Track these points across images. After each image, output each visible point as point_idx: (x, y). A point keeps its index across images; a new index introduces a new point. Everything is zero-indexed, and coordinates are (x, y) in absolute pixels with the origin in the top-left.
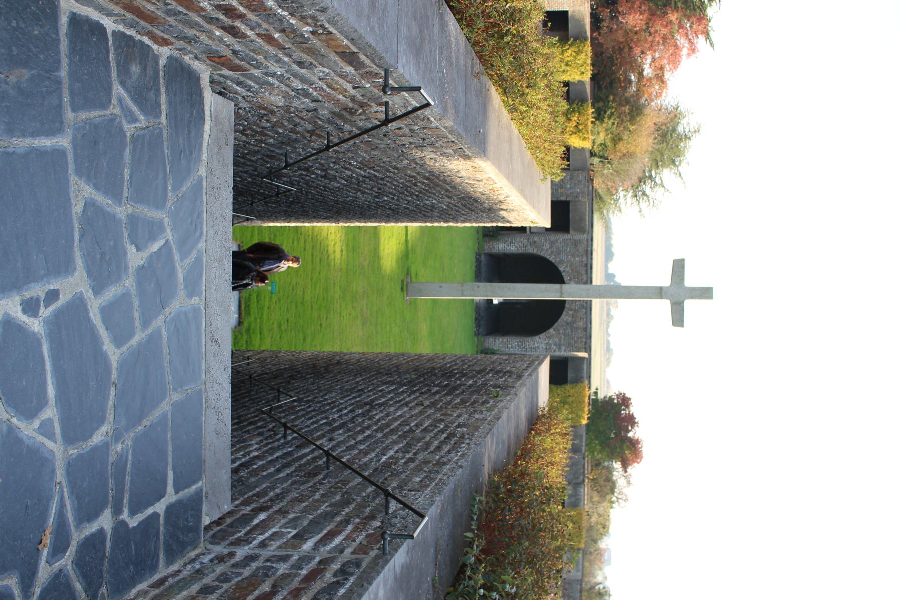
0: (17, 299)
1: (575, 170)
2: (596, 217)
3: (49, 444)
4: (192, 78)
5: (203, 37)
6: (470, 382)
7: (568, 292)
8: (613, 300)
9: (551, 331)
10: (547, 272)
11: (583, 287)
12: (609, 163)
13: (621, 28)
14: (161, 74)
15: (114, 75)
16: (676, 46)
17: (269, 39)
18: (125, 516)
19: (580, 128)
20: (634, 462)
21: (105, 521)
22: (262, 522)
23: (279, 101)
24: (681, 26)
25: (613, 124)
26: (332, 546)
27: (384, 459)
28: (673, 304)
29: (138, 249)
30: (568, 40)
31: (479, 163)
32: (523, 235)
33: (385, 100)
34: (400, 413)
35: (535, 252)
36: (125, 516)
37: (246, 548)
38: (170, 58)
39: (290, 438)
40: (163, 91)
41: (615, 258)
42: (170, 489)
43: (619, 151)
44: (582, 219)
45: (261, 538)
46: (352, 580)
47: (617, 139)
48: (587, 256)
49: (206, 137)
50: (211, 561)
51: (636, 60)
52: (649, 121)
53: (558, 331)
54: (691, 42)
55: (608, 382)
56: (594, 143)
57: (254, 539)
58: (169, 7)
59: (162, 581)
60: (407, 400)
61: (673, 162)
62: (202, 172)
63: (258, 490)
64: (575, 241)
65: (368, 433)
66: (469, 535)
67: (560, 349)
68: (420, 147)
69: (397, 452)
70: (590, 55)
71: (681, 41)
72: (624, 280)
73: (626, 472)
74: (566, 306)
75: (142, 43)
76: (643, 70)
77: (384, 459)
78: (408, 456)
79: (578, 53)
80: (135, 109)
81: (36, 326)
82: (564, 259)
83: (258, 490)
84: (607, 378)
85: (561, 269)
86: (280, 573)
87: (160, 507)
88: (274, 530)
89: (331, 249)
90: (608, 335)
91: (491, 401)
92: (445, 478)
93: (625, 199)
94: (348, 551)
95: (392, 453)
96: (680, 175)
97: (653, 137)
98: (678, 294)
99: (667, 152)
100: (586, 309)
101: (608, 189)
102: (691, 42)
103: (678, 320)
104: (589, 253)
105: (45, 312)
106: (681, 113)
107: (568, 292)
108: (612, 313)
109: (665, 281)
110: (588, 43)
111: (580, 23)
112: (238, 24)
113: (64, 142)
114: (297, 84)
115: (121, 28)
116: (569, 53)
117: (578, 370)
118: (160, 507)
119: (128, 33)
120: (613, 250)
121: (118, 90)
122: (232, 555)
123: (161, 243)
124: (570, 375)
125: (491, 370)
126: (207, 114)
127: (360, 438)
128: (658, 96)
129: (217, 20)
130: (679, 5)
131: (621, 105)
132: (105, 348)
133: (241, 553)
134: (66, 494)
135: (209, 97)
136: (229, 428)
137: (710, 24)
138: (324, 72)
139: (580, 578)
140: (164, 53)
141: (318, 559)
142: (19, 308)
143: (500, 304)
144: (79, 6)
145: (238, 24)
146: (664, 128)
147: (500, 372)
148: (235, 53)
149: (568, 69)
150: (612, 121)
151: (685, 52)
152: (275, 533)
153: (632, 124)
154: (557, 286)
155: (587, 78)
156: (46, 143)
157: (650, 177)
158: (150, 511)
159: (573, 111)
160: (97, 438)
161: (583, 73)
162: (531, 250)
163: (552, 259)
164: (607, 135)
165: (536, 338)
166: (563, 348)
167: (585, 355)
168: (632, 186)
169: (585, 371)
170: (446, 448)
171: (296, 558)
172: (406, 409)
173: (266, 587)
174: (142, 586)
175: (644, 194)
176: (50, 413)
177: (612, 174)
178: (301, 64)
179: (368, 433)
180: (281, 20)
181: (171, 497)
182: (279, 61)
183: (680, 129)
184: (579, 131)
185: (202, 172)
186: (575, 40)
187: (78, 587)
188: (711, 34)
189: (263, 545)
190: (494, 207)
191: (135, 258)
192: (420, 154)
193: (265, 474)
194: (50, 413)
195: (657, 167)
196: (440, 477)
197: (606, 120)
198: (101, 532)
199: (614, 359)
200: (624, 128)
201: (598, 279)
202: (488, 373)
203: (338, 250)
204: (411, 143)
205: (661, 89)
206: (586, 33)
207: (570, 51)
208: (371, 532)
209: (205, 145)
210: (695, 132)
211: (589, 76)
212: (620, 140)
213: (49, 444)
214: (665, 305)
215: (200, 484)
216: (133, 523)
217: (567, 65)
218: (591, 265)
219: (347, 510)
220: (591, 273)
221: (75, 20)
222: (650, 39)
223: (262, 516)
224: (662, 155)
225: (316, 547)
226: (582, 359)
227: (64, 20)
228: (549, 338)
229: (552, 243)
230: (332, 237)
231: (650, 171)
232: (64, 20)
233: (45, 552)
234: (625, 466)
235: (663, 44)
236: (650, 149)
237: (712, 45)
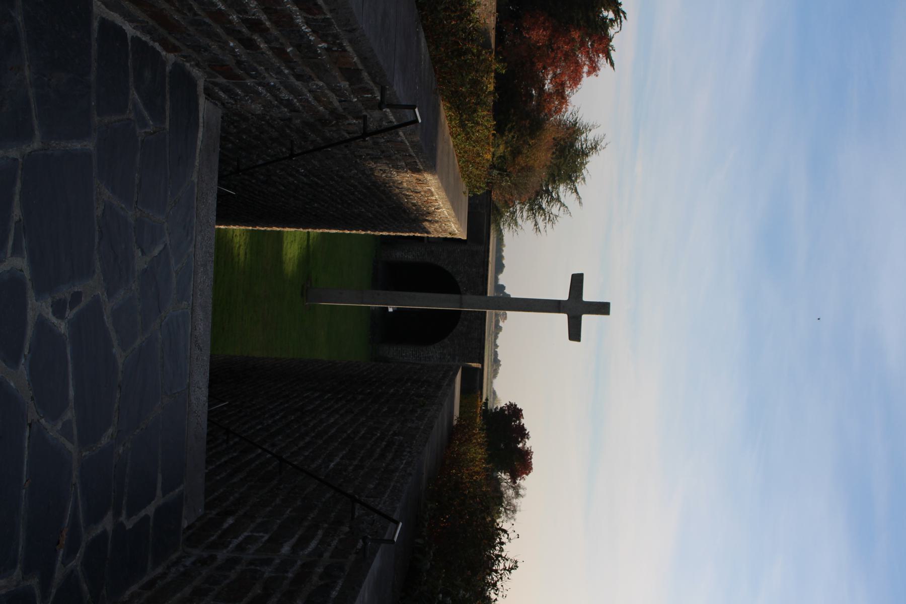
0: (49, 300)
2: (493, 227)
3: (69, 446)
4: (191, 83)
5: (214, 47)
6: (392, 391)
7: (468, 305)
8: (502, 312)
12: (507, 175)
14: (167, 79)
15: (131, 79)
16: (577, 62)
17: (280, 53)
18: (123, 519)
20: (523, 473)
21: (107, 524)
22: (231, 525)
23: (257, 108)
24: (583, 44)
25: (513, 137)
26: (309, 549)
27: (332, 465)
29: (143, 253)
31: (428, 177)
33: (365, 113)
34: (332, 420)
36: (123, 519)
37: (225, 551)
38: (175, 64)
39: (231, 443)
40: (168, 96)
41: (505, 270)
42: (159, 492)
43: (518, 164)
45: (236, 542)
46: (340, 583)
47: (516, 152)
49: (199, 143)
50: (194, 563)
51: (538, 75)
52: (549, 136)
54: (592, 61)
56: (494, 154)
57: (230, 543)
58: (196, 18)
59: (151, 584)
60: (336, 407)
61: (570, 178)
62: (195, 178)
63: (216, 494)
65: (307, 439)
66: (420, 541)
68: (376, 159)
69: (342, 458)
71: (582, 58)
72: (514, 291)
73: (515, 482)
75: (153, 48)
76: (544, 85)
77: (332, 465)
78: (355, 463)
80: (146, 114)
81: (62, 327)
83: (216, 494)
84: (504, 389)
85: (458, 279)
86: (266, 575)
87: (150, 510)
88: (246, 534)
89: (236, 251)
90: (497, 346)
91: (419, 410)
92: (399, 485)
93: (523, 215)
94: (327, 555)
95: (337, 459)
97: (551, 151)
98: (576, 308)
99: (564, 167)
101: (506, 202)
102: (592, 61)
103: (575, 334)
105: (70, 314)
106: (579, 129)
107: (468, 305)
108: (501, 324)
112: (257, 38)
113: (90, 145)
114: (285, 95)
115: (138, 34)
118: (150, 510)
119: (144, 39)
121: (134, 95)
122: (213, 558)
123: (161, 247)
126: (201, 120)
127: (301, 444)
128: (558, 111)
129: (240, 32)
130: (582, 23)
132: (114, 350)
133: (222, 555)
134: (79, 498)
135: (203, 103)
136: (206, 431)
137: (611, 44)
138: (317, 85)
140: (171, 57)
141: (299, 563)
142: (50, 310)
143: (394, 311)
144: (107, 10)
145: (257, 38)
146: (562, 143)
148: (239, 63)
151: (586, 69)
152: (248, 536)
153: (532, 138)
154: (457, 297)
156: (77, 145)
157: (547, 191)
158: (143, 513)
160: (104, 441)
164: (506, 148)
167: (479, 366)
168: (530, 199)
170: (390, 456)
171: (277, 561)
172: (337, 416)
173: (258, 590)
174: (134, 588)
175: (541, 208)
176: (70, 414)
177: (509, 186)
178: (299, 77)
179: (307, 439)
180: (303, 35)
181: (159, 500)
182: (279, 72)
183: (578, 145)
185: (195, 178)
187: (85, 587)
188: (612, 53)
189: (240, 548)
190: (421, 218)
191: (140, 262)
192: (372, 165)
193: (218, 478)
194: (70, 414)
195: (554, 182)
196: (392, 484)
198: (105, 532)
199: (501, 370)
200: (524, 141)
201: (490, 292)
203: (242, 252)
204: (368, 154)
205: (561, 104)
208: (342, 536)
209: (198, 150)
210: (592, 149)
212: (520, 153)
213: (69, 446)
214: (562, 319)
215: (181, 487)
216: (129, 525)
219: (312, 515)
221: (106, 25)
222: (552, 55)
223: (230, 521)
224: (560, 170)
225: (294, 549)
226: (476, 369)
227: (95, 24)
230: (237, 240)
231: (547, 186)
232: (95, 24)
233: (61, 552)
234: (514, 478)
235: (565, 61)
236: (548, 163)
237: (612, 64)
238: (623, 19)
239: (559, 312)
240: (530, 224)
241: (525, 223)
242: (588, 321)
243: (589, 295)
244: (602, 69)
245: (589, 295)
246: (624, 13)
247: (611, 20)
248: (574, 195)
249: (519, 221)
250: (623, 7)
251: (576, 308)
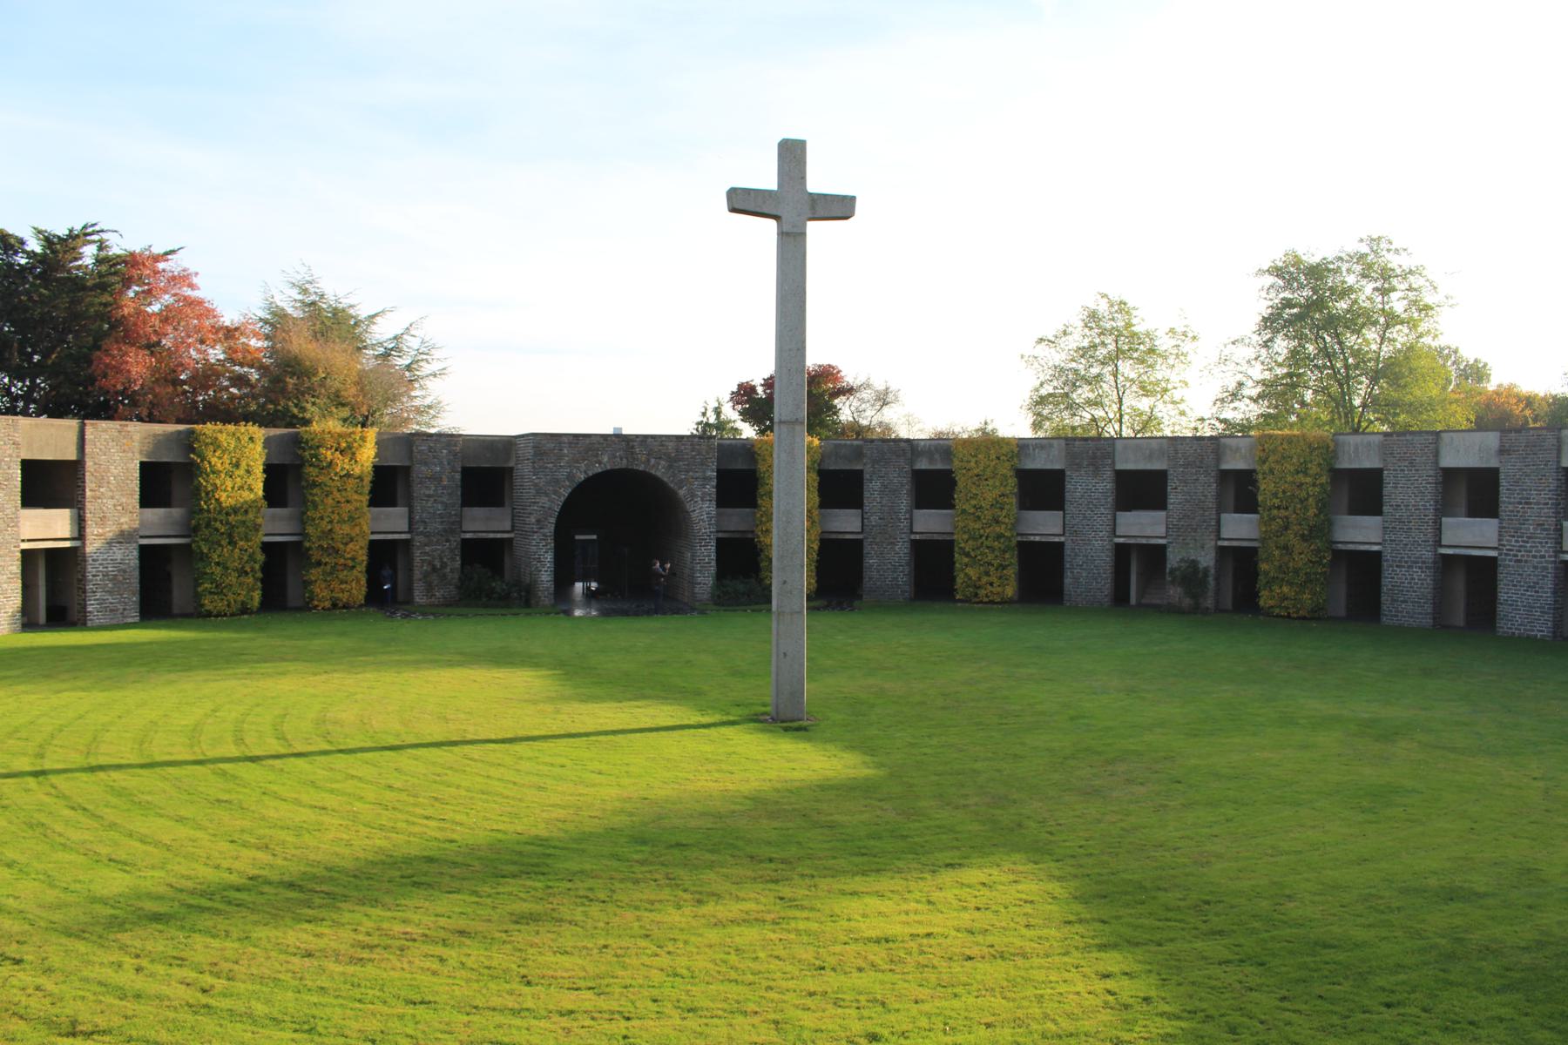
1: (411, 458)
9: (682, 492)
13: (152, 389)
19: (344, 445)
28: (783, 235)
30: (192, 463)
35: (553, 520)
53: (681, 481)
64: (535, 455)
70: (220, 426)
79: (216, 444)
82: (565, 472)
85: (583, 477)
96: (373, 316)
103: (839, 208)
110: (198, 427)
111: (161, 442)
116: (216, 461)
124: (740, 465)
131: (284, 391)
139: (1063, 443)
149: (243, 465)
150: (309, 406)
151: (188, 292)
155: (259, 433)
159: (316, 456)
161: (251, 439)
175: (408, 368)
184: (350, 447)
186: (193, 450)
197: (308, 416)
206: (179, 432)
207: (214, 460)
211: (256, 428)
214: (817, 231)
217: (237, 466)
228: (693, 496)
237: (172, 252)
238: (97, 228)
240: (431, 384)
241: (430, 391)
242: (818, 181)
243: (766, 178)
244: (185, 264)
245: (766, 178)
246: (85, 227)
247: (100, 248)
248: (378, 319)
249: (427, 402)
250: (78, 227)
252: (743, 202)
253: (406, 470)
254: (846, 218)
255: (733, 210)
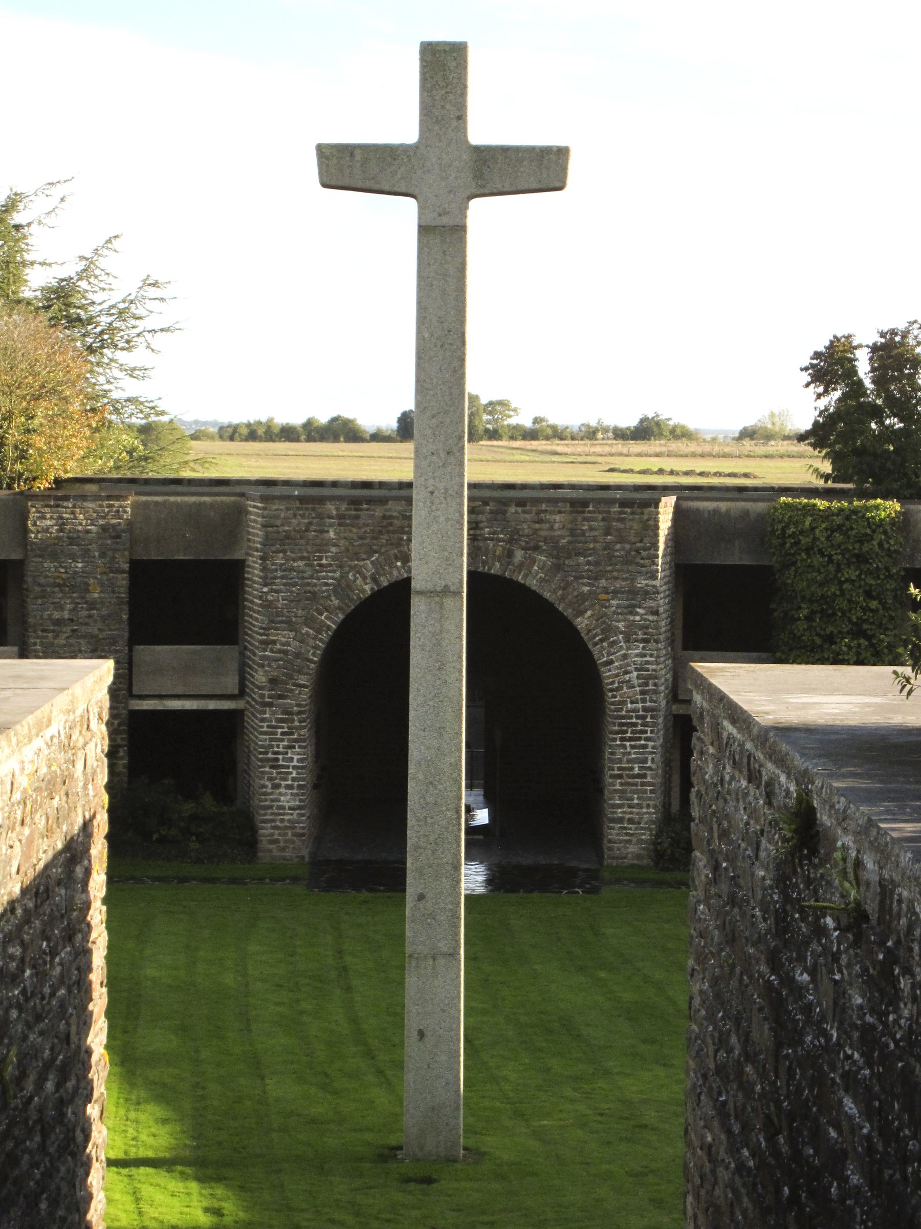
7: (440, 561)
9: (582, 623)
10: (375, 635)
11: (419, 513)
32: (251, 721)
41: (347, 414)
44: (195, 515)
48: (321, 500)
53: (583, 597)
55: (748, 434)
64: (268, 541)
67: (646, 594)
74: (496, 569)
82: (330, 578)
98: (443, 168)
100: (505, 502)
103: (538, 169)
104: (314, 494)
107: (440, 561)
108: (526, 421)
109: (399, 216)
117: (719, 529)
120: (323, 418)
125: (774, 963)
143: (490, 801)
147: (782, 925)
154: (418, 607)
162: (301, 696)
163: (331, 622)
165: (608, 674)
166: (642, 583)
169: (723, 506)
201: (394, 465)
202: (788, 981)
218: (355, 485)
220: (382, 485)
226: (678, 512)
228: (608, 631)
229: (275, 619)
239: (460, 230)
243: (398, 122)
245: (398, 122)
251: (443, 168)
252: (349, 168)
253: (20, 564)
254: (560, 189)
255: (325, 185)
